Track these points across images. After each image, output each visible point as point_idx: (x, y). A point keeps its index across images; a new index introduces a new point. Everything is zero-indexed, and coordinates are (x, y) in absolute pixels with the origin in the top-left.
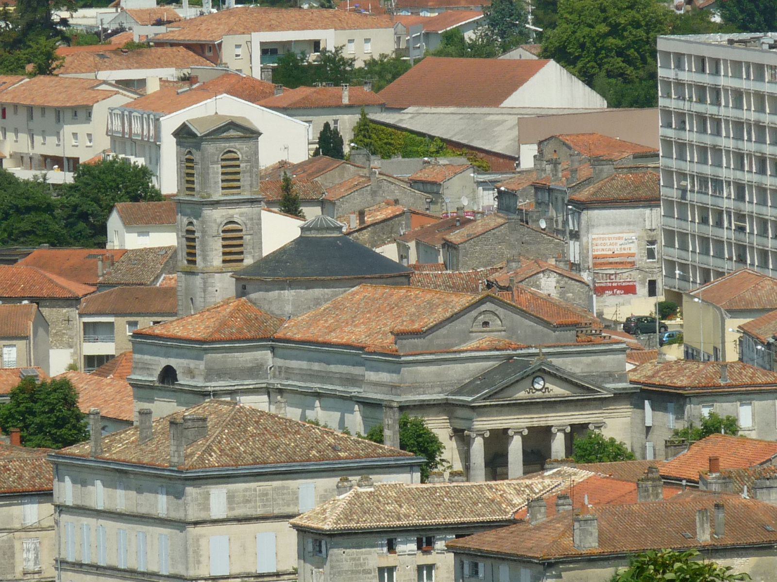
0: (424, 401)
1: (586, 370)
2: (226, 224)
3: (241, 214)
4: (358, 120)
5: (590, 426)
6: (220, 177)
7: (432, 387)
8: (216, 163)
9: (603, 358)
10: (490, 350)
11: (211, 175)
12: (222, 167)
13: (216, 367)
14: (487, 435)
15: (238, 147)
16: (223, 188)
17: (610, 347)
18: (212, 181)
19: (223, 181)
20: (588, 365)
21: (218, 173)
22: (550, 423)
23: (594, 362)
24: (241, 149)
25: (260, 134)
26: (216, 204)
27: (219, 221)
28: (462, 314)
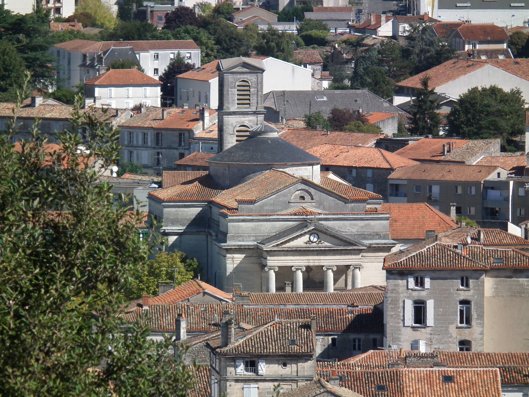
0: (241, 245)
1: (359, 230)
2: (240, 126)
3: (250, 121)
4: (167, 68)
5: (324, 268)
6: (236, 97)
7: (249, 236)
8: (234, 87)
9: (372, 223)
10: (291, 215)
11: (230, 96)
12: (238, 90)
13: (171, 218)
14: (335, 269)
15: (249, 78)
16: (238, 104)
17: (378, 216)
18: (230, 100)
19: (238, 99)
20: (362, 227)
21: (234, 94)
22: (322, 264)
23: (366, 225)
24: (251, 78)
25: (263, 71)
26: (234, 113)
27: (234, 124)
28: (318, 188)
